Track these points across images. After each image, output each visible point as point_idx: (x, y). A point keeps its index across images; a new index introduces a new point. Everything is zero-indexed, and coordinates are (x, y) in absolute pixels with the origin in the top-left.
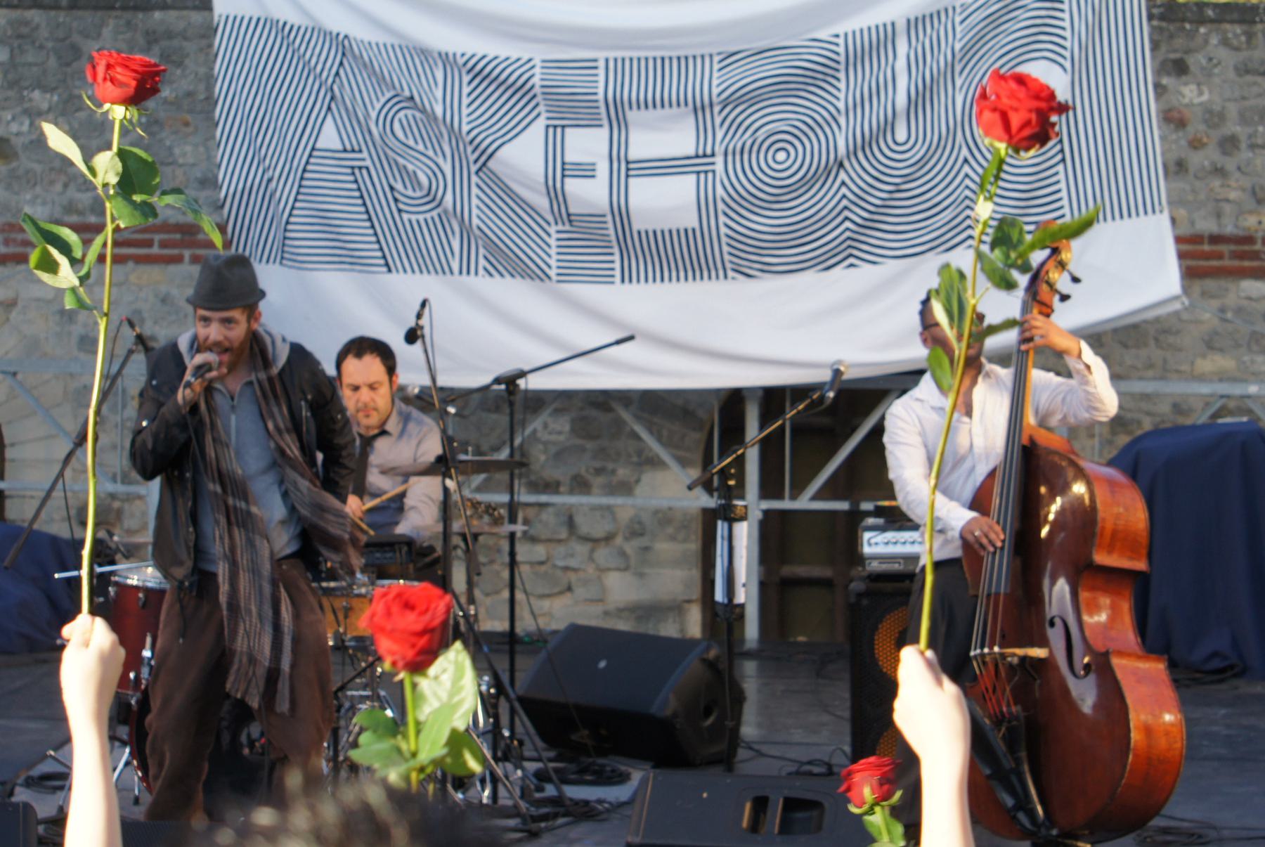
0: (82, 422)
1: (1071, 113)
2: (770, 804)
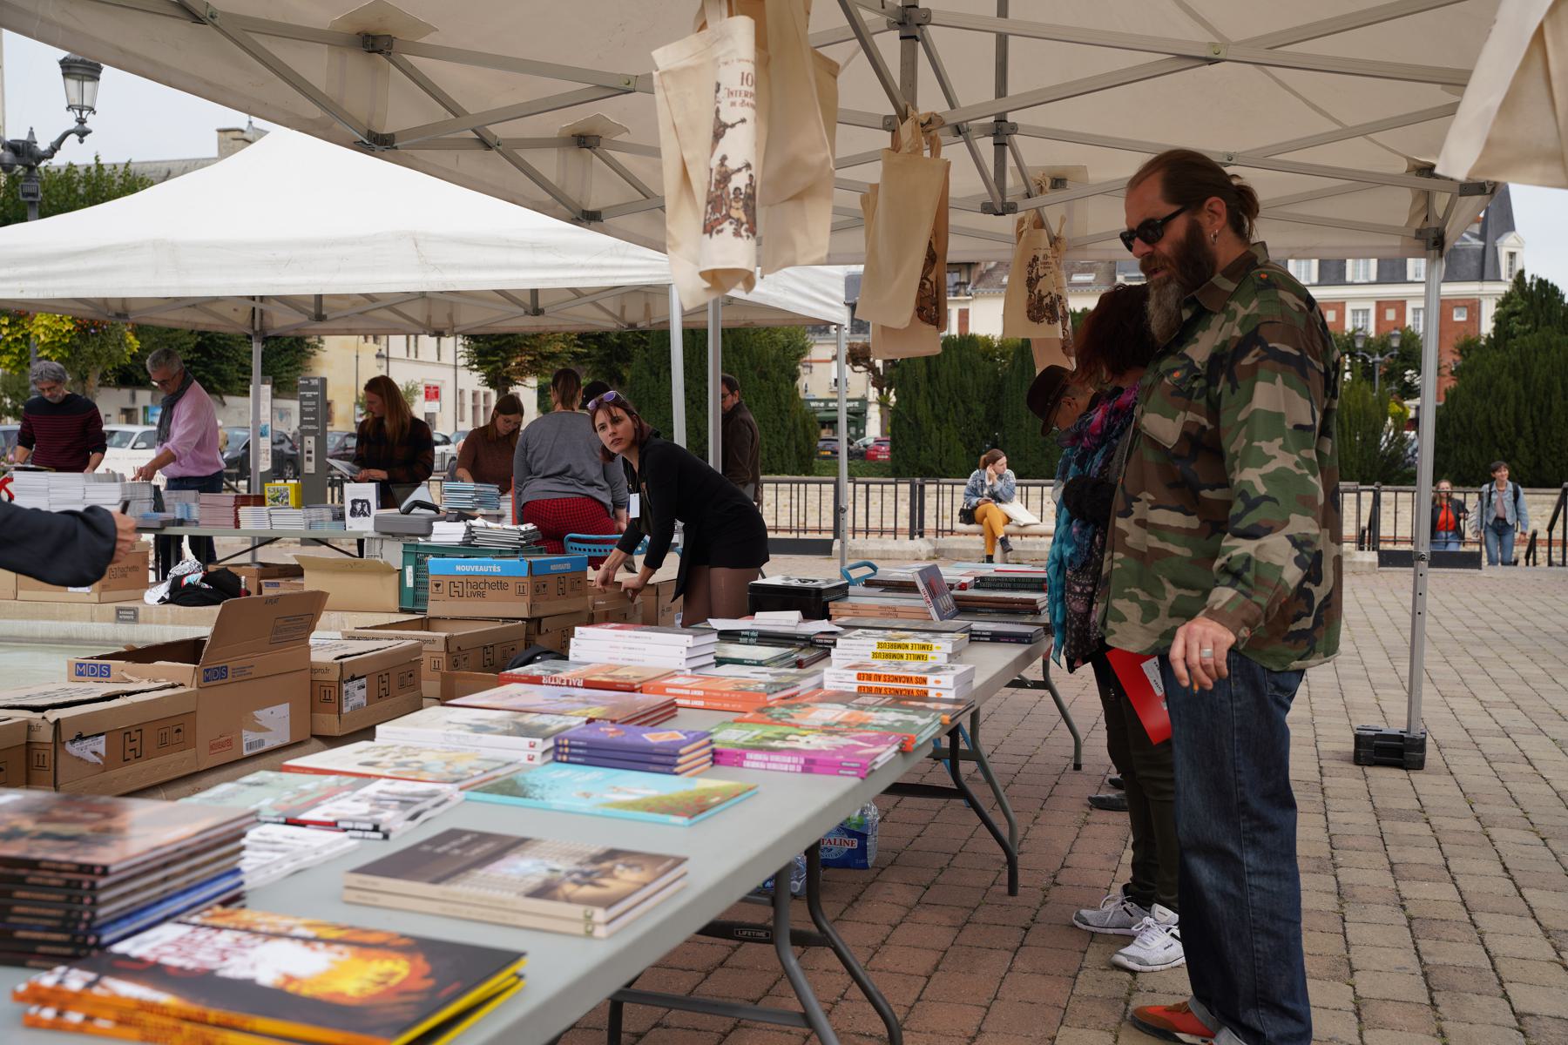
0: (130, 664)
1: (679, 701)
2: (692, 326)
